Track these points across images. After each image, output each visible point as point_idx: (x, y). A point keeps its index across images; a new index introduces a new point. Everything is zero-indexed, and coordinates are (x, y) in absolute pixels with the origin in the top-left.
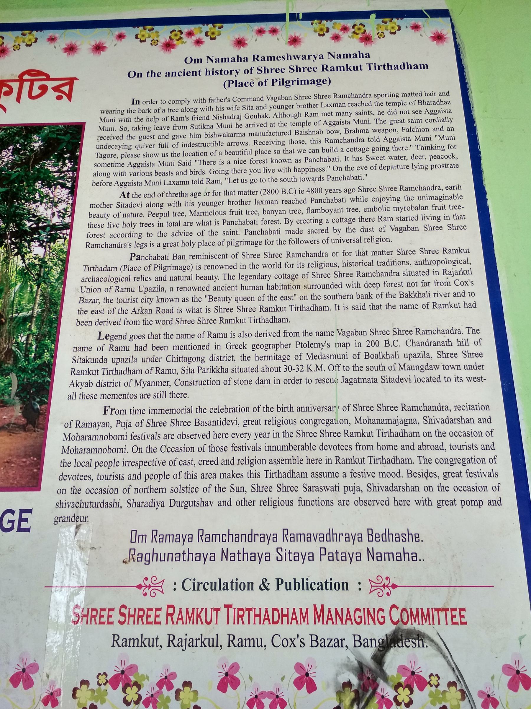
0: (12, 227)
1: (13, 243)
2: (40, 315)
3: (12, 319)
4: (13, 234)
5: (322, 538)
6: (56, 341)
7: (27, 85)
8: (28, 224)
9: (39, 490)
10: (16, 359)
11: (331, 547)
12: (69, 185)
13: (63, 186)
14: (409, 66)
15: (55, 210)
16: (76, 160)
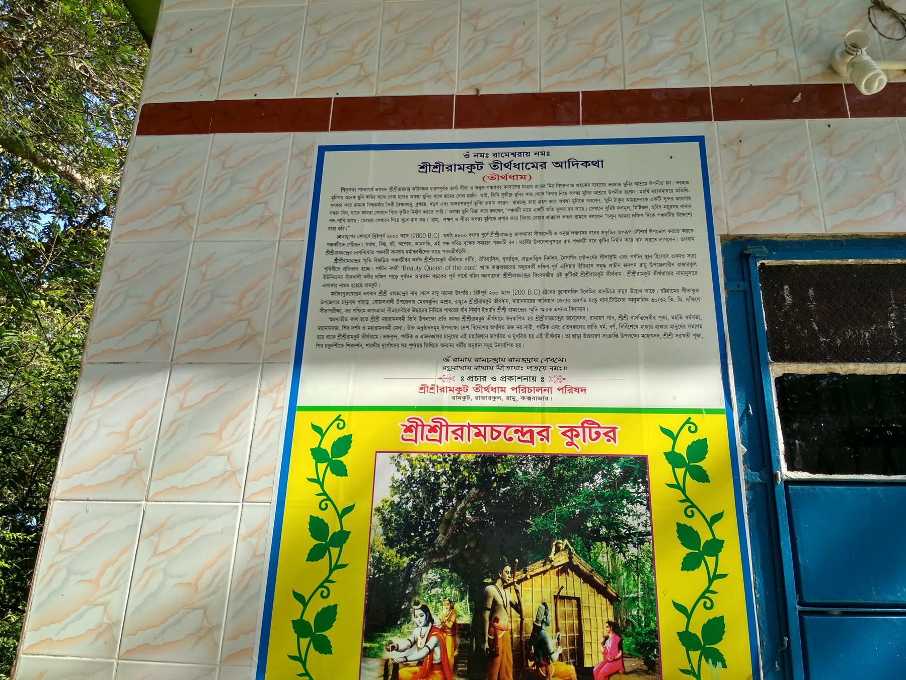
1: (615, 544)
2: (643, 596)
3: (626, 598)
6: (656, 615)
7: (587, 430)
8: (624, 531)
12: (645, 503)
13: (641, 503)
15: (639, 521)
16: (646, 484)
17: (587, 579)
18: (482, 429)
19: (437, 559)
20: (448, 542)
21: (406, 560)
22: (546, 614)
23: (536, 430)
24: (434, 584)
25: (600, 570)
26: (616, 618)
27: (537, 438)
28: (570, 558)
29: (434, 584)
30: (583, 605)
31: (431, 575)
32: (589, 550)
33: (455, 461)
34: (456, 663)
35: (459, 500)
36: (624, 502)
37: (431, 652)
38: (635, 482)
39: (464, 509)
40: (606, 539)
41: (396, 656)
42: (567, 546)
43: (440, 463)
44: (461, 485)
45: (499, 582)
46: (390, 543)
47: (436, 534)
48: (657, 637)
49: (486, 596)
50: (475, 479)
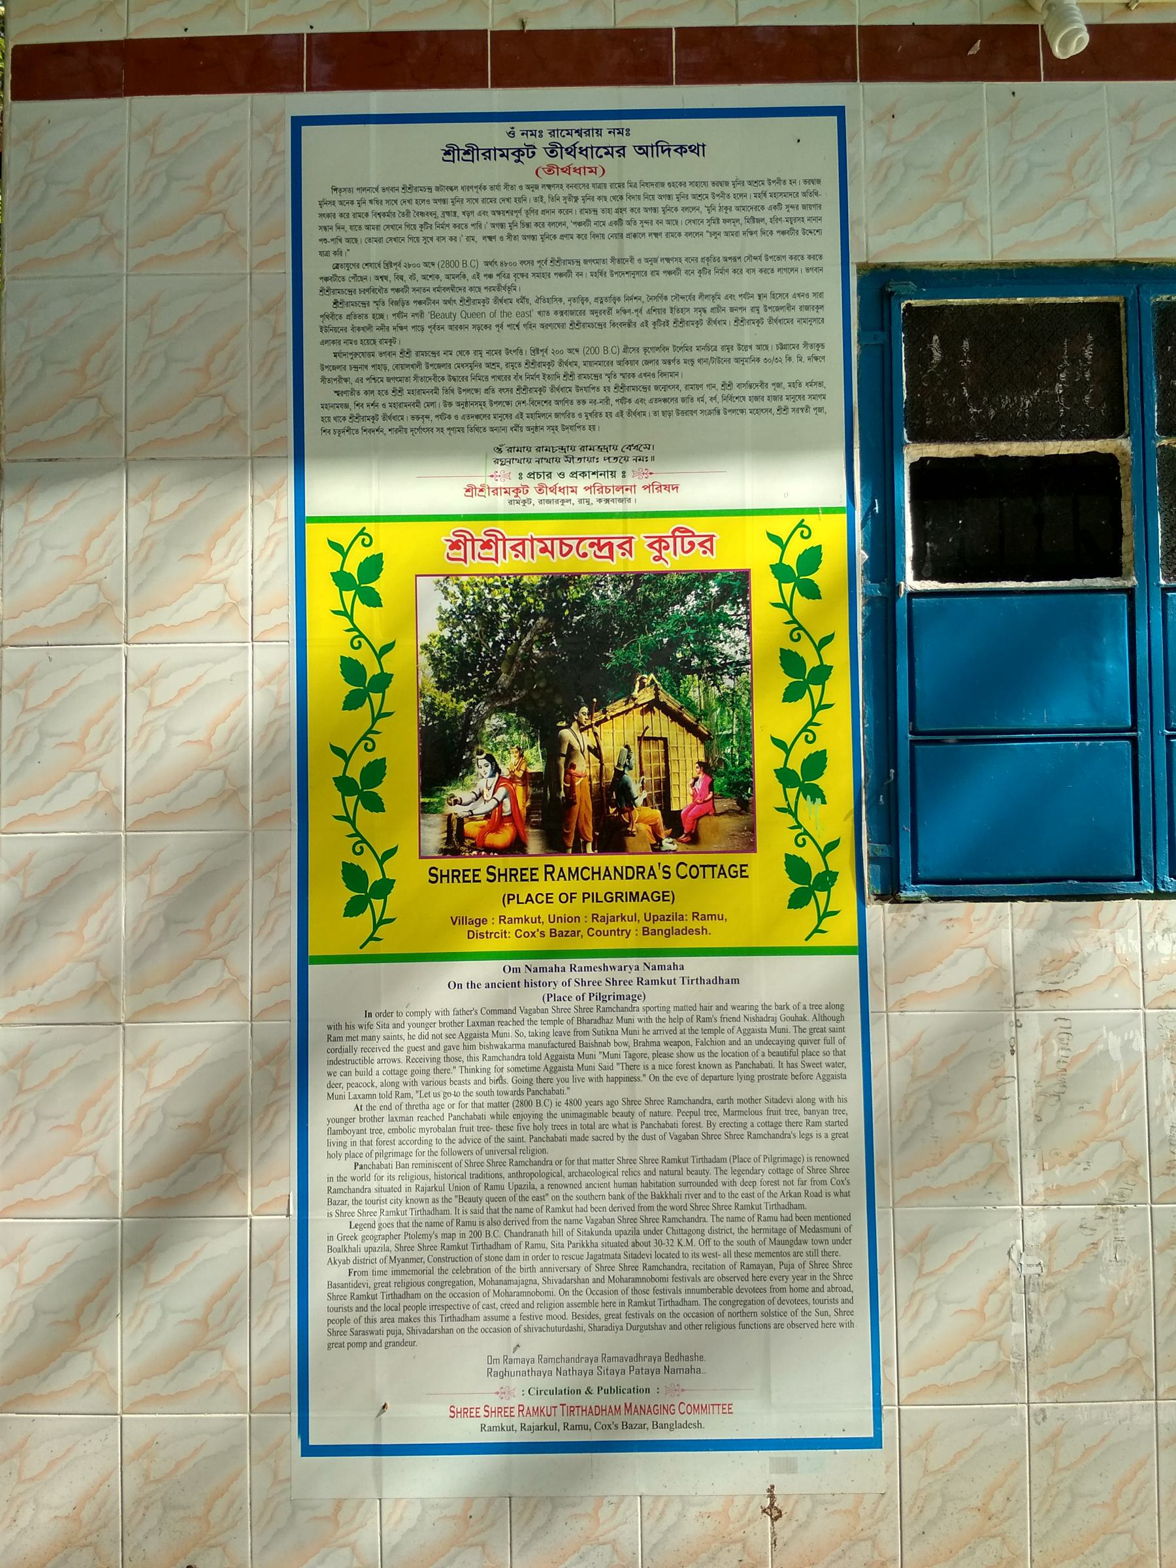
0: (706, 664)
4: (708, 669)
5: (631, 1359)
6: (752, 752)
7: (679, 540)
9: (755, 851)
10: (726, 766)
11: (638, 1365)
13: (741, 628)
14: (721, 981)
17: (676, 717)
18: (548, 543)
19: (500, 701)
20: (513, 682)
21: (464, 705)
22: (629, 757)
23: (616, 542)
24: (499, 731)
25: (690, 706)
26: (707, 758)
27: (617, 552)
28: (657, 694)
29: (499, 731)
30: (670, 745)
31: (495, 721)
32: (679, 685)
33: (516, 584)
34: (528, 814)
35: (524, 632)
36: (721, 627)
37: (500, 804)
38: (734, 602)
39: (531, 642)
40: (698, 671)
41: (460, 811)
42: (652, 682)
43: (498, 587)
44: (526, 614)
45: (575, 724)
46: (443, 686)
47: (499, 674)
48: (752, 775)
49: (560, 741)
50: (542, 607)
